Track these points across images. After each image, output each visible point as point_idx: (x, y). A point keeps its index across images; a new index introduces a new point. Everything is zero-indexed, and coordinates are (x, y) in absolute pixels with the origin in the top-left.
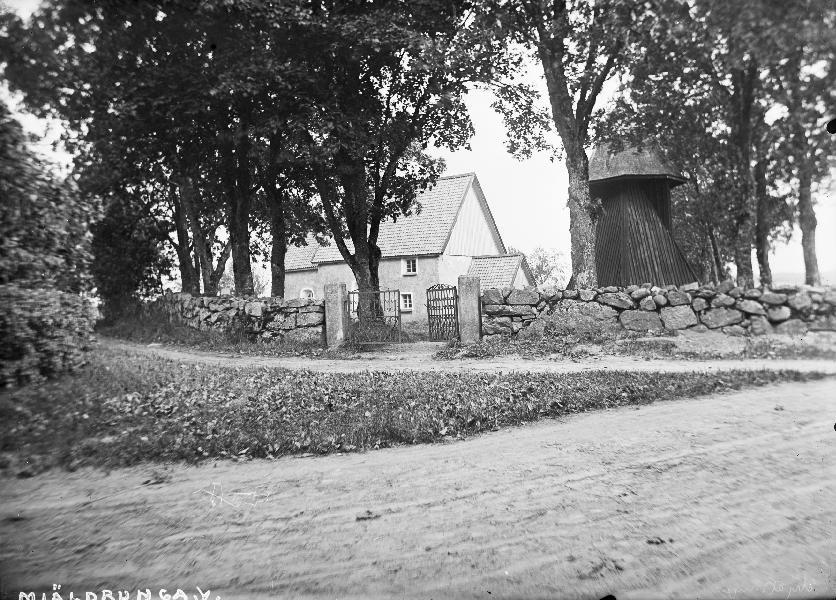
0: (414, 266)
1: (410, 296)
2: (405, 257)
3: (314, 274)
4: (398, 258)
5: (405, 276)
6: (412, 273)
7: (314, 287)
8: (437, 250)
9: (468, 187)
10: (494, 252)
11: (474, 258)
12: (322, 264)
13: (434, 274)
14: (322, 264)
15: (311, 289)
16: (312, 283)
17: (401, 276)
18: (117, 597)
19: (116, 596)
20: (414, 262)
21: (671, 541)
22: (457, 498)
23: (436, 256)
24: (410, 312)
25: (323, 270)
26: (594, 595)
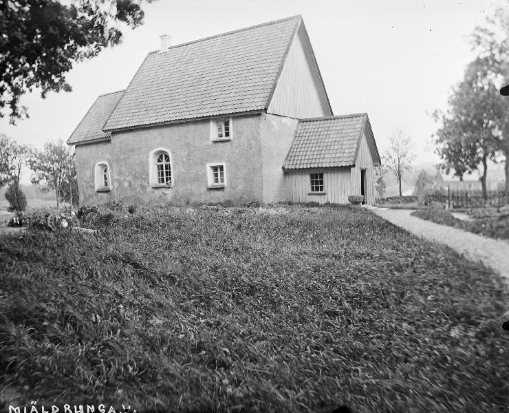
0: (227, 129)
1: (222, 168)
2: (216, 118)
3: (108, 146)
4: (205, 120)
5: (215, 142)
6: (224, 138)
7: (109, 161)
8: (258, 105)
9: (292, 38)
10: (319, 113)
11: (301, 121)
12: (115, 132)
13: (256, 139)
14: (115, 132)
15: (106, 163)
16: (107, 156)
17: (210, 142)
18: (73, 410)
19: (73, 410)
20: (227, 124)
21: (435, 115)
22: (383, 199)
23: (257, 114)
24: (222, 189)
25: (116, 140)
26: (475, 260)
